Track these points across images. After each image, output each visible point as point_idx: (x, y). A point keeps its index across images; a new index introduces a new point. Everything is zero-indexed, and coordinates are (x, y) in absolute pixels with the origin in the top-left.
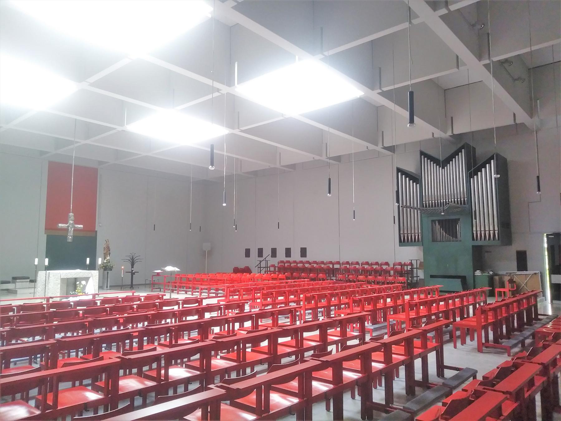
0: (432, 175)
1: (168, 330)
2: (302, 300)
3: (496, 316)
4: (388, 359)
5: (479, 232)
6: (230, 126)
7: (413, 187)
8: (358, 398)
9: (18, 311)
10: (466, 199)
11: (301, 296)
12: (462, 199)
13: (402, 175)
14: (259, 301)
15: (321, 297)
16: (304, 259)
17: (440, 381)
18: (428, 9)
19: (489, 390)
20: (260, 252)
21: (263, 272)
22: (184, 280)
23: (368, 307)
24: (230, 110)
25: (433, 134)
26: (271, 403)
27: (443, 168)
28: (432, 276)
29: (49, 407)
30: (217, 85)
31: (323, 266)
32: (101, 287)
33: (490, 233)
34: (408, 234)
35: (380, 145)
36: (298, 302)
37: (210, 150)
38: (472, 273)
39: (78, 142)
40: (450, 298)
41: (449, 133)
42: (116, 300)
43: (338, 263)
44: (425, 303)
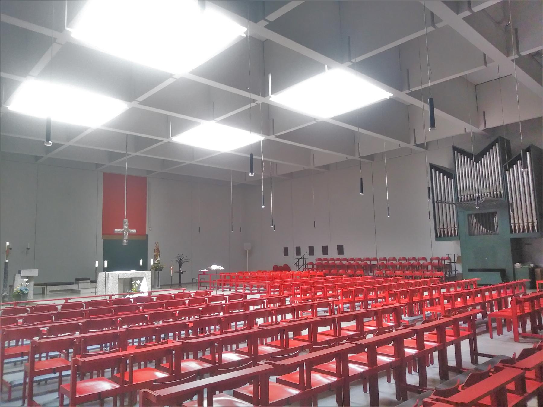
0: (466, 169)
1: (218, 321)
2: (339, 295)
3: (533, 306)
4: (420, 345)
5: (517, 225)
6: (266, 131)
7: (448, 182)
8: (393, 381)
9: (87, 307)
10: (502, 192)
11: (339, 291)
12: (498, 192)
13: (435, 171)
14: (298, 296)
15: (358, 292)
16: (341, 257)
17: (473, 367)
18: (451, 13)
19: (508, 366)
20: (298, 251)
21: (301, 270)
22: (228, 278)
23: (405, 300)
24: (264, 118)
25: (465, 129)
26: (313, 381)
27: (477, 162)
28: (470, 270)
29: (126, 383)
30: (253, 96)
31: (360, 262)
32: (153, 286)
33: (519, 226)
34: (444, 228)
35: (412, 143)
36: (336, 296)
37: (249, 156)
38: (512, 267)
39: (129, 155)
40: (486, 290)
41: (482, 127)
42: (170, 296)
43: (375, 259)
44: (461, 295)
